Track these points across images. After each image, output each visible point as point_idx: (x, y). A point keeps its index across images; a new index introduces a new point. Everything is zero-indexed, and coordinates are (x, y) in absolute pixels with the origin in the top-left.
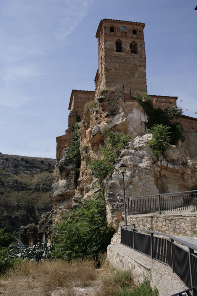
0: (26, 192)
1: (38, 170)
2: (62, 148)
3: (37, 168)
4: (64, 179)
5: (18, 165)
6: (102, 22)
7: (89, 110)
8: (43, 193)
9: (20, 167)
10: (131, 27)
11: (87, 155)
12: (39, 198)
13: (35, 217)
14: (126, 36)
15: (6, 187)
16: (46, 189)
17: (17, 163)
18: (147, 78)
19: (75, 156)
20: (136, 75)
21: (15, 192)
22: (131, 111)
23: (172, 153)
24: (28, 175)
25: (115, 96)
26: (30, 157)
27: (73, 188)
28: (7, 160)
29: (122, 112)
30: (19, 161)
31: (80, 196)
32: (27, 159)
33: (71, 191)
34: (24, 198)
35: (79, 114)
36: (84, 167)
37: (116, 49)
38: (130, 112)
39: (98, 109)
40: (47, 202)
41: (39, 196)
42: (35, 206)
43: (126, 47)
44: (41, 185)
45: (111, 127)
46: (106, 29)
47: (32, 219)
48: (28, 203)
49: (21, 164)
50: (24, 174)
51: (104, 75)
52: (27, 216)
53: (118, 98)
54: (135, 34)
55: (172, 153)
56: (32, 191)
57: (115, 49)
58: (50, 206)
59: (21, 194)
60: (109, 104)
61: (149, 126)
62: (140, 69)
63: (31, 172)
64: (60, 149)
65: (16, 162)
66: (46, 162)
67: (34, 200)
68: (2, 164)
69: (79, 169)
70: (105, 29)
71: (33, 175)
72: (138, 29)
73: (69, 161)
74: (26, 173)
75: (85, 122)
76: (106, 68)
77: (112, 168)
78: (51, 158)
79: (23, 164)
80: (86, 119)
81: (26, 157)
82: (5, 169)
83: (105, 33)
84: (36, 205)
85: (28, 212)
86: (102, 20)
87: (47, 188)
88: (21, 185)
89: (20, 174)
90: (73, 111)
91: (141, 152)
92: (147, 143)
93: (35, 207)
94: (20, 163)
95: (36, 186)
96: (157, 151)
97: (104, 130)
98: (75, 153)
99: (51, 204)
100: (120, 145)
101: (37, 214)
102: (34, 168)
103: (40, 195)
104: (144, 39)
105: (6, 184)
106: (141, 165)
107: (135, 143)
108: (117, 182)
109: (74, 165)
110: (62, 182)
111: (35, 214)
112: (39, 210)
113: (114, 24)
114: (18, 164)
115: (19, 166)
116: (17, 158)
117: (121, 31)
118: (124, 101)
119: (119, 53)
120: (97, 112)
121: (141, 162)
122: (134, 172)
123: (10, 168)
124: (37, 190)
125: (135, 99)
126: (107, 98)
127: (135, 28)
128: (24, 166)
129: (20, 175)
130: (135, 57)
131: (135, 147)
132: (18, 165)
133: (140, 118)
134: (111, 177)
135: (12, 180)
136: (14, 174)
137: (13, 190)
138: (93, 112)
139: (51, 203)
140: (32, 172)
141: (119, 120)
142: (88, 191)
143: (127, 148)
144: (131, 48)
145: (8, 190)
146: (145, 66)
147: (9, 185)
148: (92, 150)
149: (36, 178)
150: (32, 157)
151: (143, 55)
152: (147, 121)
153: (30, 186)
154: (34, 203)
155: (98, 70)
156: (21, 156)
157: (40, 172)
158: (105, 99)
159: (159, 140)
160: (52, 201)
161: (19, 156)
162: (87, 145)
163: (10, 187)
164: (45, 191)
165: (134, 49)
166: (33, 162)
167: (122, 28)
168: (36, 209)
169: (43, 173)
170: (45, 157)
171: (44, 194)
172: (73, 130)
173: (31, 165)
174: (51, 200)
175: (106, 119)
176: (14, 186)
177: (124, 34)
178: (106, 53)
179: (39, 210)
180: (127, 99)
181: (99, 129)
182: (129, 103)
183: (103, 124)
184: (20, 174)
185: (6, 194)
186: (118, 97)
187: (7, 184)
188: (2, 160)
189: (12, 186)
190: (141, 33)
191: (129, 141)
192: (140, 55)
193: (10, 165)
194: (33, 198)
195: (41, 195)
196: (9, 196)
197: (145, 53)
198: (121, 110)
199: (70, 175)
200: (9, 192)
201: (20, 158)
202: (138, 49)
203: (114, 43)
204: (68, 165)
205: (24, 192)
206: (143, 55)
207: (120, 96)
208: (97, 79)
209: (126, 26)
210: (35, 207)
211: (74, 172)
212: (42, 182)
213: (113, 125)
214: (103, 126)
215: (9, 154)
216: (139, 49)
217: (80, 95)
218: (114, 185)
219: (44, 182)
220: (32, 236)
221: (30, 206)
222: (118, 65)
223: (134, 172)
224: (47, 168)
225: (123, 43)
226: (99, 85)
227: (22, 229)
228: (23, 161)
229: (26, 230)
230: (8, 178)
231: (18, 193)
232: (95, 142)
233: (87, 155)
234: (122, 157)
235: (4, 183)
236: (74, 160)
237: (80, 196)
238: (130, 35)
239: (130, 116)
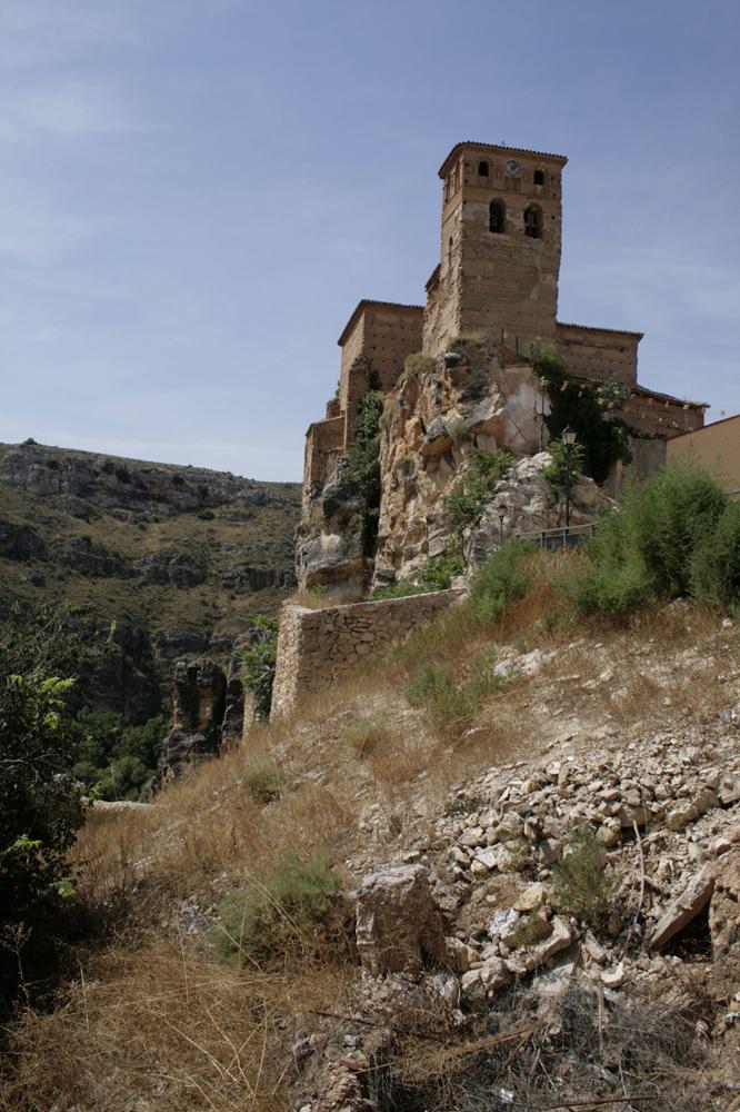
0: (120, 581)
1: (162, 507)
2: (326, 454)
3: (160, 499)
4: (335, 533)
5: (93, 487)
6: (458, 150)
7: (416, 375)
8: (179, 587)
9: (98, 494)
10: (530, 166)
11: (408, 478)
12: (166, 604)
13: (150, 667)
14: (516, 190)
15: (52, 563)
16: (189, 574)
17: (90, 479)
18: (559, 302)
19: (366, 478)
20: (534, 295)
21: (84, 578)
22: (514, 390)
23: (582, 492)
24: (126, 524)
25: (483, 354)
26: (133, 460)
27: (357, 554)
28: (53, 465)
29: (496, 392)
30: (97, 474)
31: (391, 568)
32: (126, 467)
33: (352, 562)
34: (112, 601)
35: (375, 367)
36: (398, 507)
38: (511, 393)
39: (442, 378)
40: (193, 620)
41: (166, 598)
42: (150, 630)
43: (516, 221)
44: (174, 561)
45: (471, 424)
46: (470, 169)
47: (141, 674)
48: (129, 619)
49: (102, 483)
50: (112, 519)
51: (456, 290)
52: (124, 662)
53: (488, 359)
55: (582, 492)
56: (141, 579)
57: (487, 224)
58: (202, 636)
59: (104, 586)
60: (469, 371)
61: (555, 425)
62: (544, 280)
63: (138, 515)
64: (322, 455)
65: (87, 478)
66: (192, 481)
67: (148, 610)
68: (38, 479)
69: (376, 510)
70: (465, 169)
71: (144, 523)
72: (549, 171)
73: (348, 489)
74: (119, 517)
75: (405, 402)
76: (462, 273)
77: (481, 510)
78: (210, 468)
79: (111, 485)
80: (408, 393)
81: (119, 459)
82: (46, 499)
83: (466, 181)
84: (154, 628)
85: (128, 650)
86: (460, 144)
87: (194, 572)
88: (102, 558)
89: (100, 517)
90: (362, 360)
91: (529, 487)
92: (540, 471)
93: (149, 633)
94: (98, 479)
95: (157, 565)
96: (558, 488)
97: (456, 431)
98: (368, 469)
99: (206, 629)
100: (494, 471)
101: (158, 658)
102: (149, 500)
103: (169, 596)
104: (560, 199)
105: (52, 551)
106: (528, 509)
107: (520, 470)
108: (488, 532)
109: (363, 499)
110: (331, 540)
111: (150, 657)
112: (163, 646)
113: (490, 156)
114: (94, 483)
115: (97, 490)
116: (90, 461)
117: (506, 174)
118: (503, 367)
119: (495, 235)
120: (440, 385)
121: (528, 504)
122: (516, 519)
123: (64, 496)
124: (159, 577)
125: (526, 360)
126: (465, 359)
127: (542, 166)
128: (112, 492)
129: (99, 523)
130: (535, 248)
131: (520, 477)
132: (93, 487)
133: (533, 406)
134: (477, 524)
135: (75, 538)
136: (77, 516)
137: (74, 571)
138: (430, 384)
139: (206, 624)
140: (141, 514)
141: (488, 411)
142: (411, 556)
143: (507, 479)
144: (526, 220)
145: (59, 571)
146: (558, 271)
147: (60, 556)
148: (424, 470)
149: (154, 535)
150: (140, 462)
151: (554, 242)
152: (548, 412)
153: (135, 562)
154: (148, 620)
155: (439, 267)
156: (105, 455)
157: (170, 516)
158: (461, 359)
159: (563, 468)
160: (208, 619)
161: (98, 455)
162: (407, 457)
163: (67, 562)
164: (185, 581)
165: (533, 231)
166: (145, 479)
167: (509, 168)
168: (154, 640)
169: (179, 519)
170: (187, 465)
171: (182, 594)
172: (361, 410)
173: (139, 491)
174: (208, 615)
175: (460, 405)
176: (80, 560)
177: (512, 184)
178: (465, 235)
179: (163, 644)
180: (508, 362)
181: (444, 427)
182: (512, 370)
183: (453, 417)
184: (100, 517)
185: (53, 585)
187: (55, 551)
188: (36, 466)
189: (73, 557)
190: (555, 183)
191: (509, 466)
192: (548, 242)
193: (65, 484)
194: (142, 605)
195: (173, 595)
196: (63, 592)
197: (559, 238)
198: (493, 388)
199: (350, 524)
200: (61, 578)
201: (99, 462)
202: (545, 227)
204: (346, 499)
205: (114, 581)
206: (554, 242)
207: (492, 356)
208: (434, 284)
209: (519, 161)
210: (149, 633)
211: (361, 517)
212: (175, 551)
213: (474, 421)
214: (452, 421)
215: (61, 446)
216: (546, 226)
217: (380, 316)
218: (485, 536)
219: (181, 553)
220: (209, 690)
221: (135, 630)
222: (491, 266)
223: (516, 519)
224: (195, 502)
225: (508, 210)
226: (441, 307)
227: (180, 670)
228: (110, 473)
229: (193, 672)
230: (59, 530)
231: (94, 583)
232: (432, 454)
233: (408, 478)
234: (497, 492)
235: (43, 547)
236: (363, 487)
237: (391, 568)
238: (528, 186)
239: (512, 400)
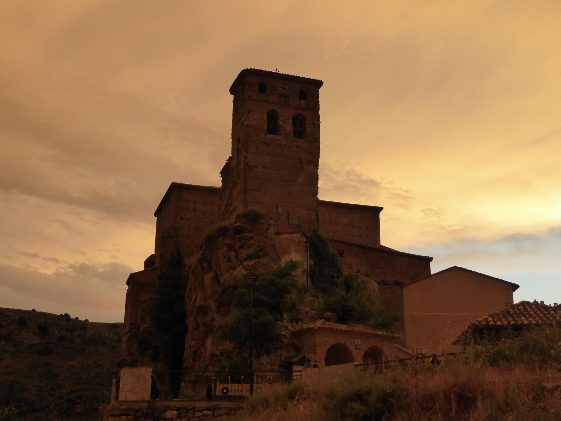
37: (266, 129)
53: (267, 228)
54: (304, 99)
57: (265, 128)
186: (266, 226)
203: (265, 116)
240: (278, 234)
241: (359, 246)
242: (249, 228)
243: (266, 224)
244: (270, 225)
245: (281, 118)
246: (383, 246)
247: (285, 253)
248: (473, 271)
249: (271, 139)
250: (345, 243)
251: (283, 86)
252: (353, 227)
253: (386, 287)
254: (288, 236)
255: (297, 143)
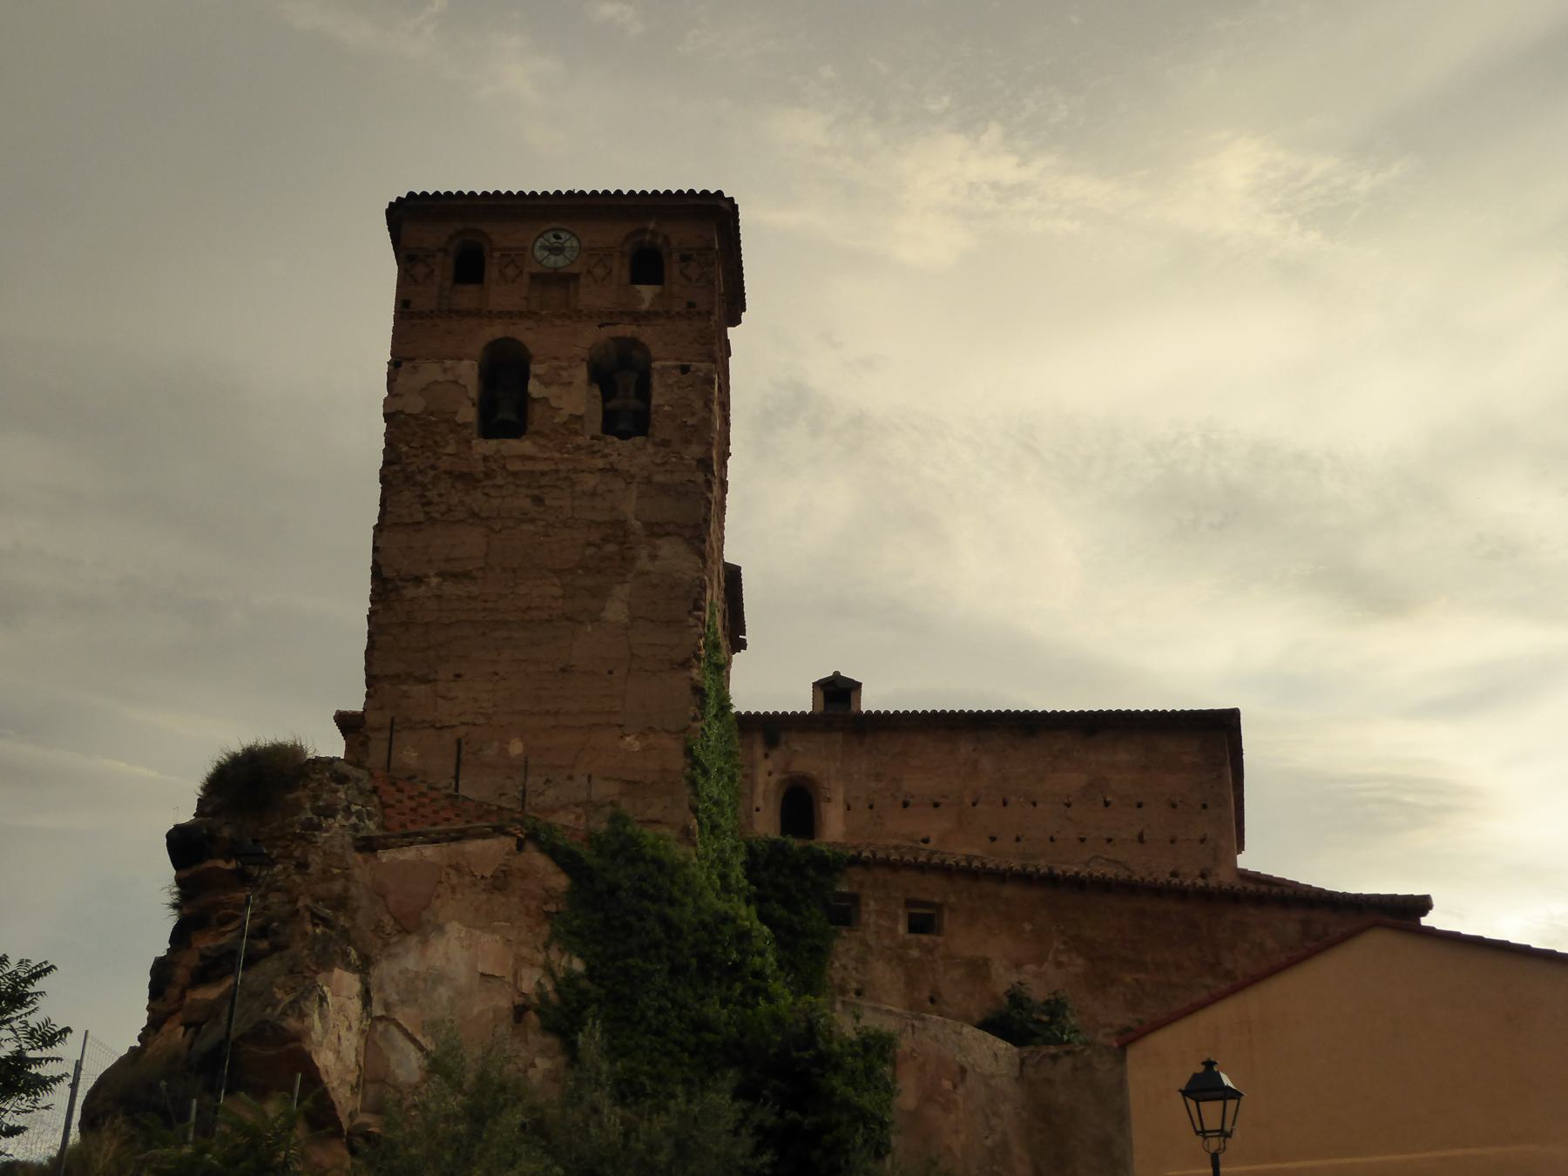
186: (310, 815)
203: (468, 371)
240: (367, 846)
241: (1025, 878)
242: (226, 832)
243: (308, 806)
244: (328, 812)
245: (535, 368)
246: (1246, 870)
247: (405, 931)
248: (1441, 931)
249: (485, 459)
250: (947, 871)
251: (553, 240)
252: (1107, 804)
253: (1053, 1049)
254: (429, 851)
255: (605, 456)
